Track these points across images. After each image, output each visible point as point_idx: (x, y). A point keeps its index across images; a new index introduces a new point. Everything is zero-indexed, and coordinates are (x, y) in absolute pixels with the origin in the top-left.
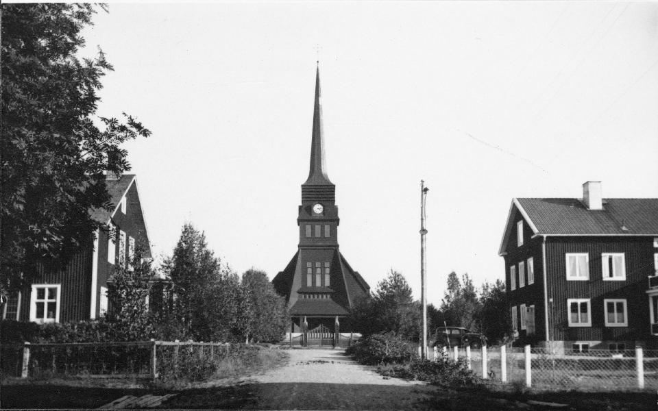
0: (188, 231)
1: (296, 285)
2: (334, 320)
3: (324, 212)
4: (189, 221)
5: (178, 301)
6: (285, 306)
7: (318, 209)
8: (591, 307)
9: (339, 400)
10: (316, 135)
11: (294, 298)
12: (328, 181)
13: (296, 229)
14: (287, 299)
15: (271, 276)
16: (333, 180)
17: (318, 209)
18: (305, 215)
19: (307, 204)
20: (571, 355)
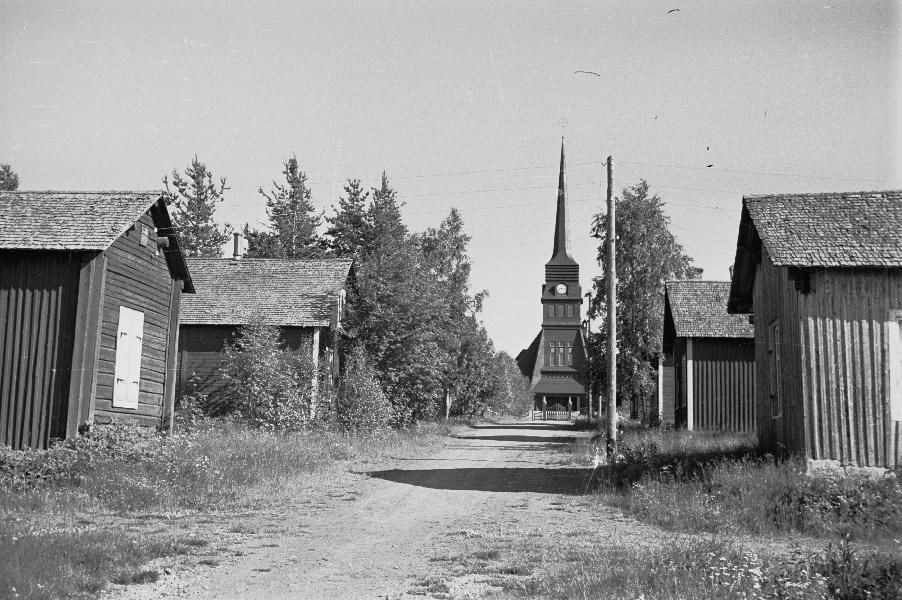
0: (455, 220)
1: (540, 363)
2: (542, 399)
3: (567, 293)
4: (455, 206)
5: (333, 363)
6: (528, 387)
7: (561, 289)
8: (664, 392)
9: (609, 575)
10: (560, 239)
11: (537, 379)
12: (572, 260)
13: (539, 309)
14: (531, 379)
15: (514, 354)
16: (577, 262)
17: (561, 289)
18: (549, 299)
19: (551, 285)
20: (313, 342)
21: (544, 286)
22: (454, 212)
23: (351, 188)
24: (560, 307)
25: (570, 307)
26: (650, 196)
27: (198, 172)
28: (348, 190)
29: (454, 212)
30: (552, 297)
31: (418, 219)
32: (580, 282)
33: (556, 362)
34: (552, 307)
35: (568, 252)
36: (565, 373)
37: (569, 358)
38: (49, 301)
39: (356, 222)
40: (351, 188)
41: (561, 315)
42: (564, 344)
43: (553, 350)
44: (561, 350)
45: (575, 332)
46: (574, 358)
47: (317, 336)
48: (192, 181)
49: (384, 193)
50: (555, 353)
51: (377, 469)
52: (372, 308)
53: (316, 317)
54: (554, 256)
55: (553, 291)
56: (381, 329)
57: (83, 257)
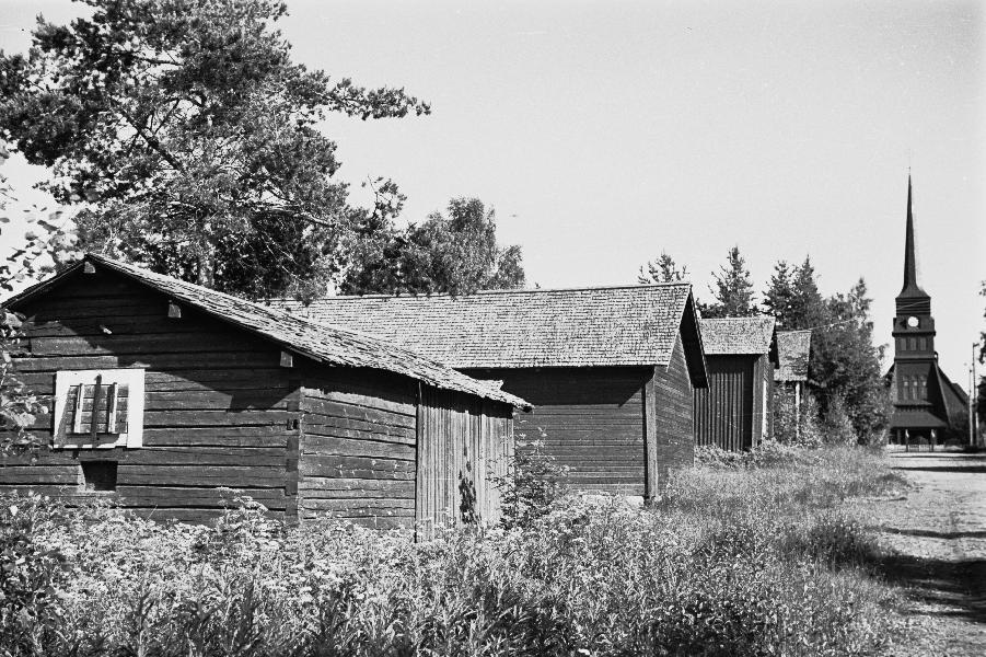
3: (919, 326)
7: (913, 322)
12: (924, 293)
17: (913, 322)
21: (895, 320)
22: (861, 281)
23: (780, 268)
24: (913, 340)
25: (923, 341)
26: (76, 22)
27: (667, 262)
28: (777, 269)
29: (861, 281)
30: (903, 331)
31: (829, 288)
32: (932, 315)
33: (910, 397)
34: (903, 340)
35: (919, 284)
36: (920, 407)
37: (924, 393)
38: (738, 380)
39: (785, 293)
40: (780, 268)
41: (923, 348)
42: (917, 377)
43: (906, 384)
44: (916, 384)
45: (928, 366)
46: (929, 392)
47: (798, 388)
48: (661, 270)
49: (807, 270)
50: (908, 387)
51: (459, 366)
52: (837, 366)
53: (797, 374)
54: (904, 290)
55: (904, 324)
56: (844, 380)
57: (756, 357)
